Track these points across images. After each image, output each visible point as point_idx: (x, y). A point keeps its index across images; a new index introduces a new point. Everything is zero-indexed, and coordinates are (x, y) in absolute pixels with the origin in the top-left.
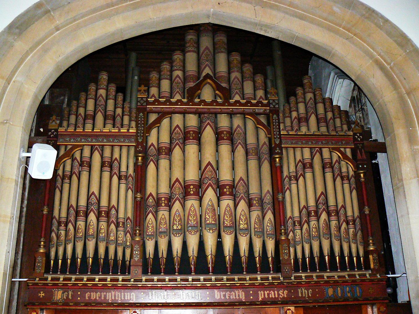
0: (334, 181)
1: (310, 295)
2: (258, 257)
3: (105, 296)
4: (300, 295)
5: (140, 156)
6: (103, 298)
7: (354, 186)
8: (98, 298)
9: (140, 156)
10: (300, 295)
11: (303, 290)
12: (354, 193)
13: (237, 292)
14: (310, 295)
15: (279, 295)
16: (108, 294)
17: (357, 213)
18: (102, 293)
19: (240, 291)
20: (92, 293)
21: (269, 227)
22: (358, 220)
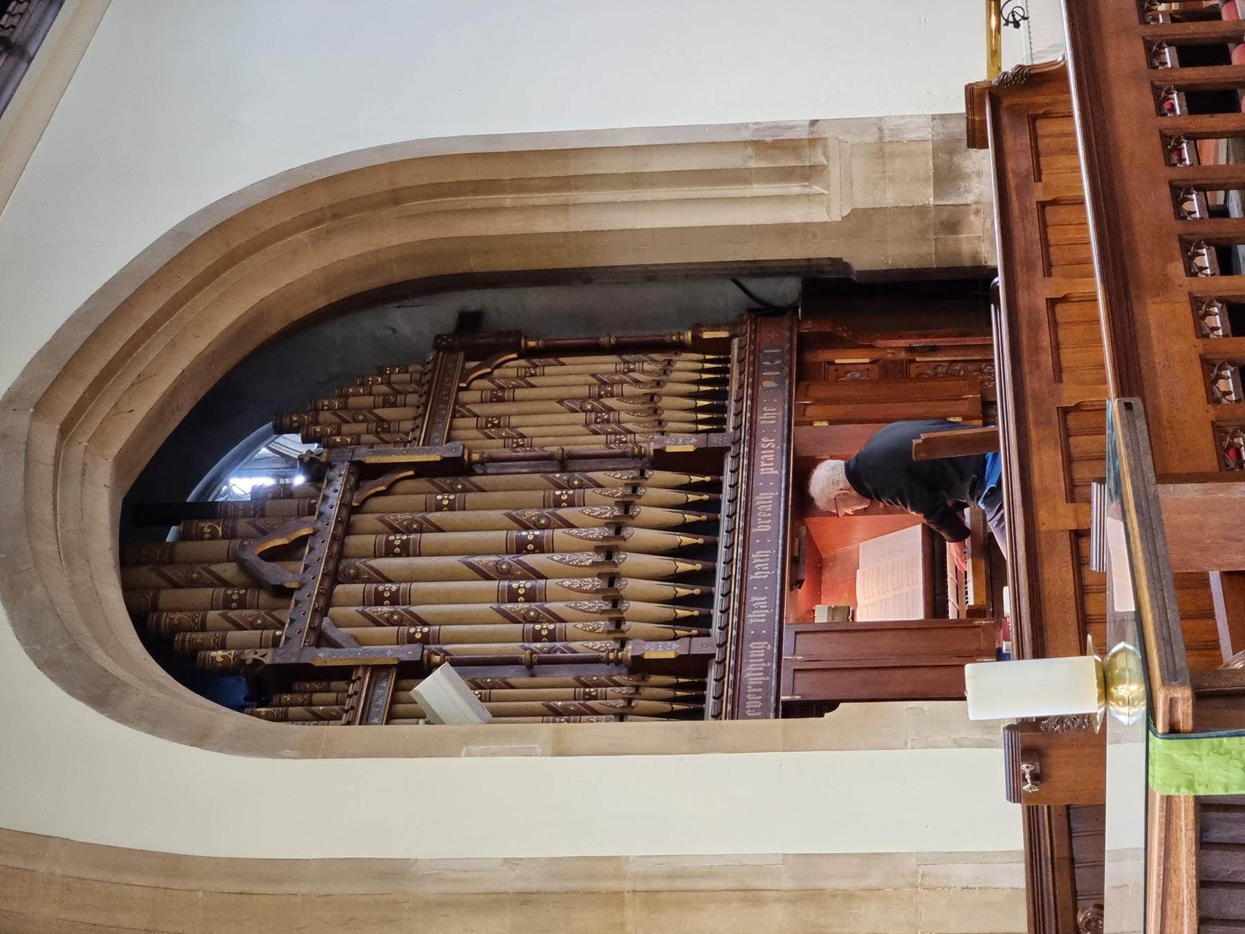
0: (533, 386)
1: (774, 409)
2: (677, 611)
3: (755, 686)
4: (763, 620)
5: (526, 344)
6: (760, 690)
7: (551, 360)
8: (760, 697)
9: (526, 344)
10: (773, 422)
11: (749, 669)
12: (563, 359)
13: (758, 503)
14: (774, 409)
15: (769, 448)
16: (750, 683)
17: (613, 358)
18: (749, 691)
19: (754, 556)
20: (748, 707)
21: (623, 475)
22: (626, 357)
